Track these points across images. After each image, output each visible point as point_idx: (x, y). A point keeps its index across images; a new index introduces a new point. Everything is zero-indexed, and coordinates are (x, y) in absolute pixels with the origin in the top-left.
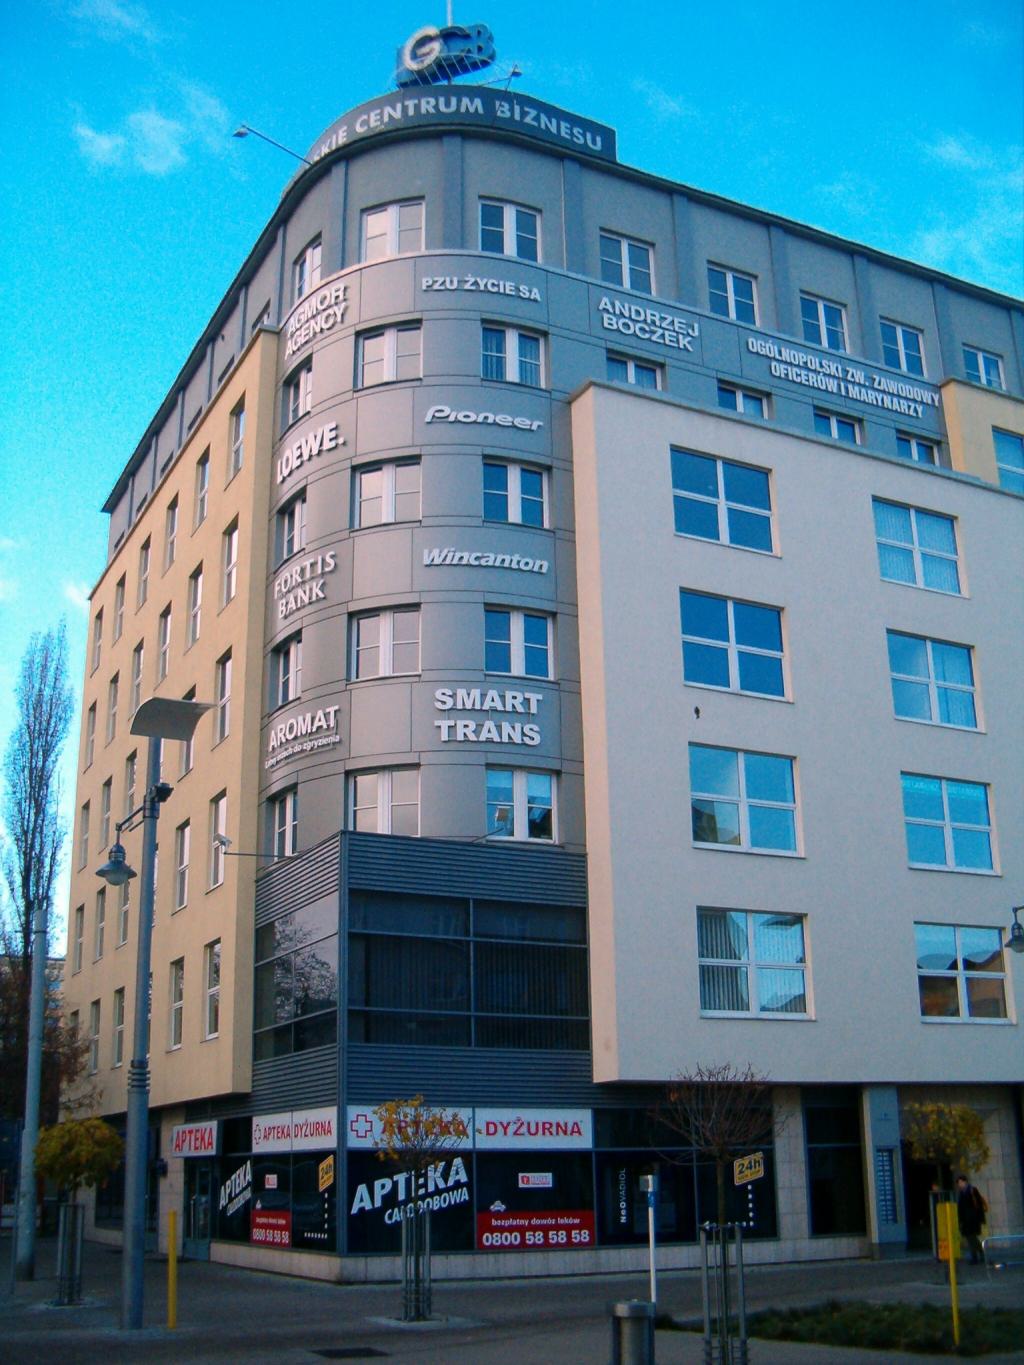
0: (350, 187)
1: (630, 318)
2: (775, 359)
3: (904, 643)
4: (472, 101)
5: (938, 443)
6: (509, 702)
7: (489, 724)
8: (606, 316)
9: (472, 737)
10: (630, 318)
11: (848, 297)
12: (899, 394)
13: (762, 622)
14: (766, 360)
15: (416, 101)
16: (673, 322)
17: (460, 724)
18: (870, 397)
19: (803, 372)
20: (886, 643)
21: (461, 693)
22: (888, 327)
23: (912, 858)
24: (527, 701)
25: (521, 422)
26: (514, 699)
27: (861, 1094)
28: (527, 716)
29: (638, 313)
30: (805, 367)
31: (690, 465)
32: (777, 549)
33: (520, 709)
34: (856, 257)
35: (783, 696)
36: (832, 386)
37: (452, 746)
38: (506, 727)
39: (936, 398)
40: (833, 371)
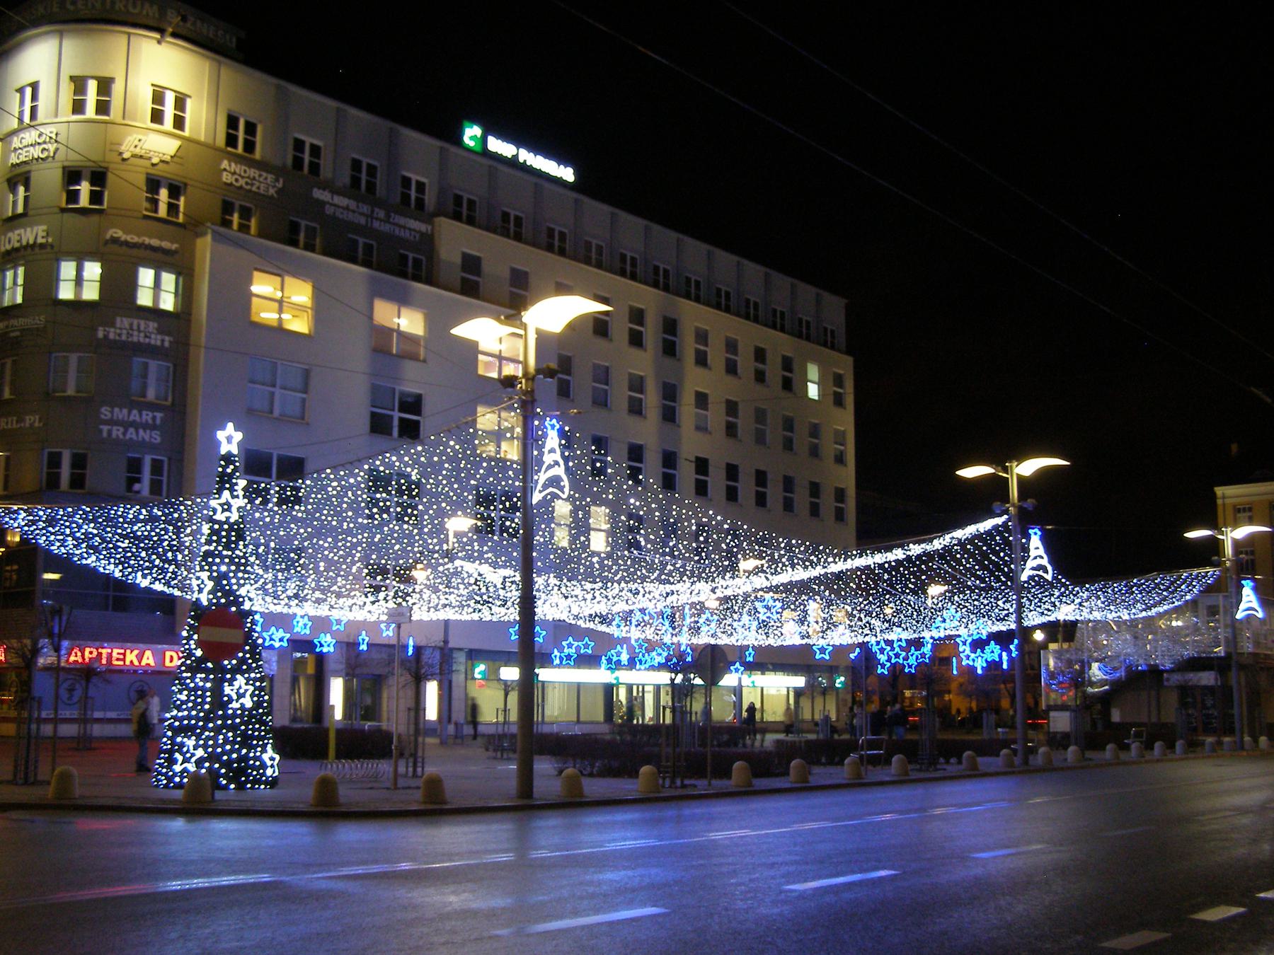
1: (240, 175)
2: (328, 203)
4: (121, 411)
6: (144, 417)
9: (121, 436)
15: (109, 651)
16: (266, 179)
17: (115, 428)
19: (345, 212)
25: (166, 245)
27: (542, 735)
28: (153, 427)
29: (245, 171)
36: (363, 221)
38: (141, 432)
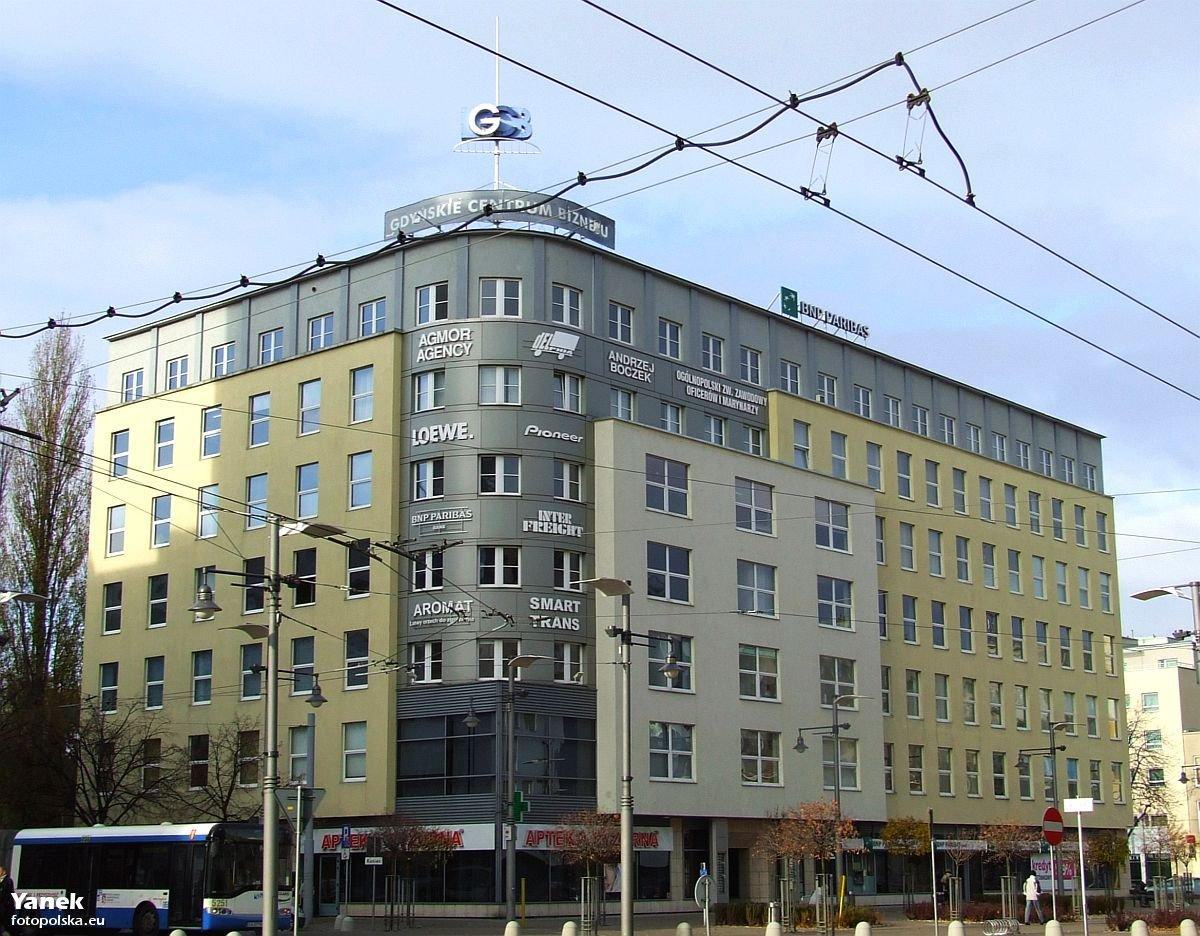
0: (471, 291)
1: (623, 364)
3: (744, 567)
5: (763, 430)
7: (557, 619)
8: (612, 363)
9: (549, 626)
10: (623, 364)
11: (764, 347)
12: (744, 401)
13: (681, 558)
14: (683, 385)
18: (733, 403)
20: (645, 461)
21: (544, 600)
22: (744, 349)
23: (741, 693)
24: (574, 605)
26: (568, 605)
30: (703, 387)
31: (654, 464)
32: (690, 514)
33: (571, 610)
34: (732, 305)
35: (687, 601)
37: (530, 535)
39: (765, 399)
40: (716, 389)
